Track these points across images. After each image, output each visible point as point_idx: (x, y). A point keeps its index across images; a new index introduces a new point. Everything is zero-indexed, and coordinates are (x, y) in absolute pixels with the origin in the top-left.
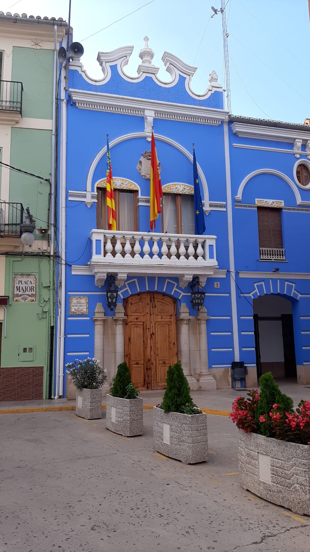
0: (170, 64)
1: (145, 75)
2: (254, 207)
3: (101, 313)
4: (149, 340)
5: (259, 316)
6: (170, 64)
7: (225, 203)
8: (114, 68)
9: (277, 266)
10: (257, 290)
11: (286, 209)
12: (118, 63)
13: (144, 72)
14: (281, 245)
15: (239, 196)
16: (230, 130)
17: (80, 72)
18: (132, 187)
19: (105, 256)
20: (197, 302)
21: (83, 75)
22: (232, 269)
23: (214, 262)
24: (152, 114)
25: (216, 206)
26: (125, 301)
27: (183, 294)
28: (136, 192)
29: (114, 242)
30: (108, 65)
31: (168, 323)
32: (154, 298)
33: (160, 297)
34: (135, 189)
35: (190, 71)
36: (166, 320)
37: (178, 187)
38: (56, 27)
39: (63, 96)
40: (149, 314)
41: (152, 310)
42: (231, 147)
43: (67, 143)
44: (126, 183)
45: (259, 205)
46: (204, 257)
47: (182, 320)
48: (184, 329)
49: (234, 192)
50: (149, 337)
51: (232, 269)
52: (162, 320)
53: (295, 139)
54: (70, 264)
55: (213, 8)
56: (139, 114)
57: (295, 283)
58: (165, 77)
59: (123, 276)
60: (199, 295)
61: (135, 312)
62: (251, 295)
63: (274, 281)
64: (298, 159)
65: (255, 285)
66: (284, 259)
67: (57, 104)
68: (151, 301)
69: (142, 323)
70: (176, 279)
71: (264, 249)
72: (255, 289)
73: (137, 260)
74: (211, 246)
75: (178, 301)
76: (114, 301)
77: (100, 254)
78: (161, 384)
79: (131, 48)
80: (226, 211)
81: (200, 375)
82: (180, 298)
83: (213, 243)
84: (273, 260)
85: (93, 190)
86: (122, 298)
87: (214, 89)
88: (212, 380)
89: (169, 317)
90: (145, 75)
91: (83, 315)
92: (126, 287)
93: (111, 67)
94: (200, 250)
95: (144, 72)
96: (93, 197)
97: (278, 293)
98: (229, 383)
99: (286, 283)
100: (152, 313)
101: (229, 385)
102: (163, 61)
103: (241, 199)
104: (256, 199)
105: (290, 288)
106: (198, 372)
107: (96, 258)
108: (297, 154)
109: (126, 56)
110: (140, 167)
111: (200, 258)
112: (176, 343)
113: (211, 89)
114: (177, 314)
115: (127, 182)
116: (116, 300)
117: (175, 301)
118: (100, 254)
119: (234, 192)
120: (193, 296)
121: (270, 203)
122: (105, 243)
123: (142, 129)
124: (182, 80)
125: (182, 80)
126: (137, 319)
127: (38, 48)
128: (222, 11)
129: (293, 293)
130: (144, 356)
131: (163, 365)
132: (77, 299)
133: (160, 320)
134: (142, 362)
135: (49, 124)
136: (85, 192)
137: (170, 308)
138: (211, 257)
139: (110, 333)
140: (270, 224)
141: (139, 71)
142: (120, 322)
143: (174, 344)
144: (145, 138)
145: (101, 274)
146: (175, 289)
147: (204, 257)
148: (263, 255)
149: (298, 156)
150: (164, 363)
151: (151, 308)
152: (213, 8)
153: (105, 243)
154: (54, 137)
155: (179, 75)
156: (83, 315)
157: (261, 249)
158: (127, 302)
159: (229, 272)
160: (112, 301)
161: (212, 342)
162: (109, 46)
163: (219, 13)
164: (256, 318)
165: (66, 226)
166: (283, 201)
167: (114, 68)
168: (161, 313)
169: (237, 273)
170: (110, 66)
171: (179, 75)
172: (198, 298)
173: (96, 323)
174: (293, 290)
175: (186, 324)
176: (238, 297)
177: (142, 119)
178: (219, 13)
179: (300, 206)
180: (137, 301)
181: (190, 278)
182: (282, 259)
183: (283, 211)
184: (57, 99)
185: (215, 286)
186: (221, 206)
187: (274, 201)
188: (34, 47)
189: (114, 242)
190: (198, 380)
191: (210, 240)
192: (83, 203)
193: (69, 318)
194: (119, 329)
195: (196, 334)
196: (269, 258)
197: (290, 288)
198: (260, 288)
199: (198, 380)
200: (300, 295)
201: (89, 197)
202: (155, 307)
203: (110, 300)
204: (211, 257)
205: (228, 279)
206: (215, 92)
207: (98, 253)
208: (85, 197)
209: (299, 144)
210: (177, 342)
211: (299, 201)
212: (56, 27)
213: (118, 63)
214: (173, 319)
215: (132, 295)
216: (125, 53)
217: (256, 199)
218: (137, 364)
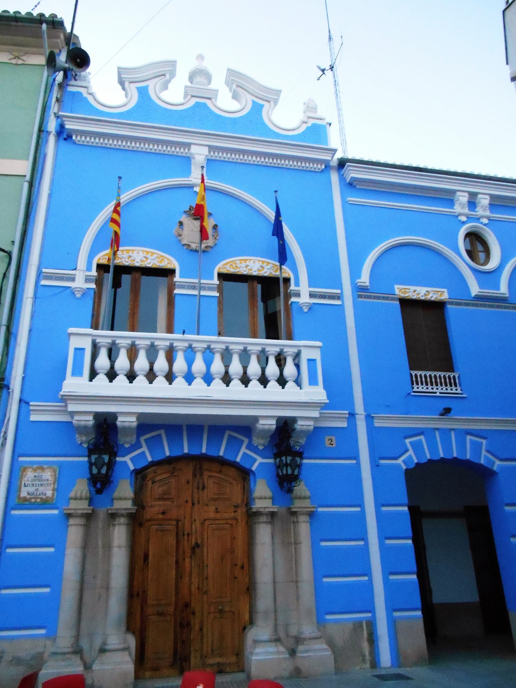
0: (238, 86)
1: (194, 101)
2: (393, 299)
3: (81, 499)
4: (187, 560)
5: (422, 508)
6: (238, 86)
7: (339, 291)
8: (143, 92)
9: (447, 404)
10: (411, 452)
11: (452, 303)
12: (151, 84)
13: (192, 96)
14: (451, 369)
15: (365, 279)
16: (342, 178)
17: (85, 95)
18: (165, 264)
19: (91, 380)
20: (285, 472)
21: (90, 99)
22: (359, 409)
23: (318, 394)
24: (205, 151)
25: (323, 296)
26: (140, 475)
27: (260, 460)
28: (170, 272)
29: (112, 353)
30: (134, 86)
31: (230, 522)
32: (201, 468)
33: (216, 467)
34: (169, 266)
35: (272, 96)
36: (226, 515)
37: (251, 264)
38: (44, 26)
39: (52, 125)
40: (190, 504)
41: (196, 495)
42: (344, 203)
43: (50, 196)
44: (153, 257)
45: (402, 295)
46: (298, 382)
47: (258, 514)
48: (264, 533)
49: (355, 273)
50: (188, 551)
51: (359, 409)
52: (218, 516)
53: (454, 192)
54: (27, 400)
55: (319, 68)
56: (181, 151)
57: (485, 438)
58: (226, 103)
59: (127, 421)
60: (289, 459)
61: (160, 499)
62: (400, 461)
63: (446, 433)
64: (464, 223)
65: (407, 441)
66: (459, 391)
67: (39, 137)
68: (194, 475)
69: (174, 523)
70: (244, 428)
71: (419, 373)
72: (407, 451)
73: (160, 388)
74: (311, 361)
75: (252, 477)
76: (104, 471)
77: (81, 374)
78: (211, 661)
79: (173, 64)
80: (342, 306)
81: (298, 640)
82: (254, 468)
83: (316, 355)
84: (438, 394)
85: (89, 269)
86: (132, 467)
87: (311, 122)
88: (325, 650)
89: (233, 509)
90: (194, 101)
91: (45, 503)
92: (141, 447)
93: (139, 89)
94: (289, 369)
95: (192, 96)
96: (88, 280)
97: (455, 458)
98: (364, 656)
99: (469, 437)
100: (196, 502)
101: (364, 661)
102: (228, 85)
103: (367, 284)
104: (396, 287)
105: (476, 448)
106: (293, 631)
107: (74, 384)
108: (460, 214)
109: (163, 75)
110: (180, 232)
111: (290, 385)
112: (246, 566)
113: (306, 120)
114: (248, 500)
115: (155, 256)
116: (108, 469)
117: (245, 474)
118: (81, 374)
119: (355, 273)
120: (278, 460)
121: (420, 292)
122: (94, 357)
123: (188, 172)
124: (257, 109)
125: (257, 109)
126: (163, 513)
127: (20, 62)
128: (332, 68)
129: (483, 458)
130: (177, 594)
131: (218, 615)
132: (35, 470)
133: (212, 515)
134: (171, 609)
135: (24, 167)
136: (73, 272)
137: (236, 493)
138: (313, 381)
139: (100, 544)
140: (427, 332)
141: (186, 95)
142: (122, 520)
143: (242, 567)
144: (191, 187)
145: (84, 415)
146: (243, 450)
147: (298, 382)
148: (417, 384)
149: (464, 219)
150: (221, 612)
151: (196, 491)
152: (319, 68)
153: (94, 357)
154: (26, 186)
155: (253, 101)
156: (45, 503)
157: (414, 373)
158: (144, 478)
159: (352, 415)
160: (99, 472)
161: (324, 565)
162: (136, 58)
163: (328, 73)
164: (416, 514)
165: (30, 331)
166: (445, 290)
167: (143, 92)
168: (216, 500)
169: (369, 418)
170: (138, 89)
171: (253, 101)
172: (286, 465)
173: (72, 521)
174: (484, 453)
175: (265, 522)
176: (375, 466)
177: (188, 159)
178: (328, 73)
179: (478, 298)
180: (164, 476)
181: (271, 424)
182: (454, 391)
183: (449, 306)
184: (40, 130)
185: (327, 443)
186: (332, 297)
187: (429, 289)
188: (14, 61)
189: (112, 353)
190: (293, 653)
191: (310, 349)
192: (68, 291)
193: (14, 512)
194: (120, 535)
195: (289, 544)
196: (430, 390)
197: (476, 448)
198: (417, 447)
199: (293, 653)
200: (498, 462)
201: (82, 279)
202: (204, 488)
203: (95, 471)
204: (313, 381)
205: (351, 431)
206: (314, 125)
207: (77, 372)
208: (73, 279)
209: (463, 198)
210: (249, 564)
211: (475, 289)
212: (44, 26)
213: (151, 84)
214: (241, 512)
215: (153, 464)
216: (165, 71)
217: (396, 287)
218: (160, 614)
